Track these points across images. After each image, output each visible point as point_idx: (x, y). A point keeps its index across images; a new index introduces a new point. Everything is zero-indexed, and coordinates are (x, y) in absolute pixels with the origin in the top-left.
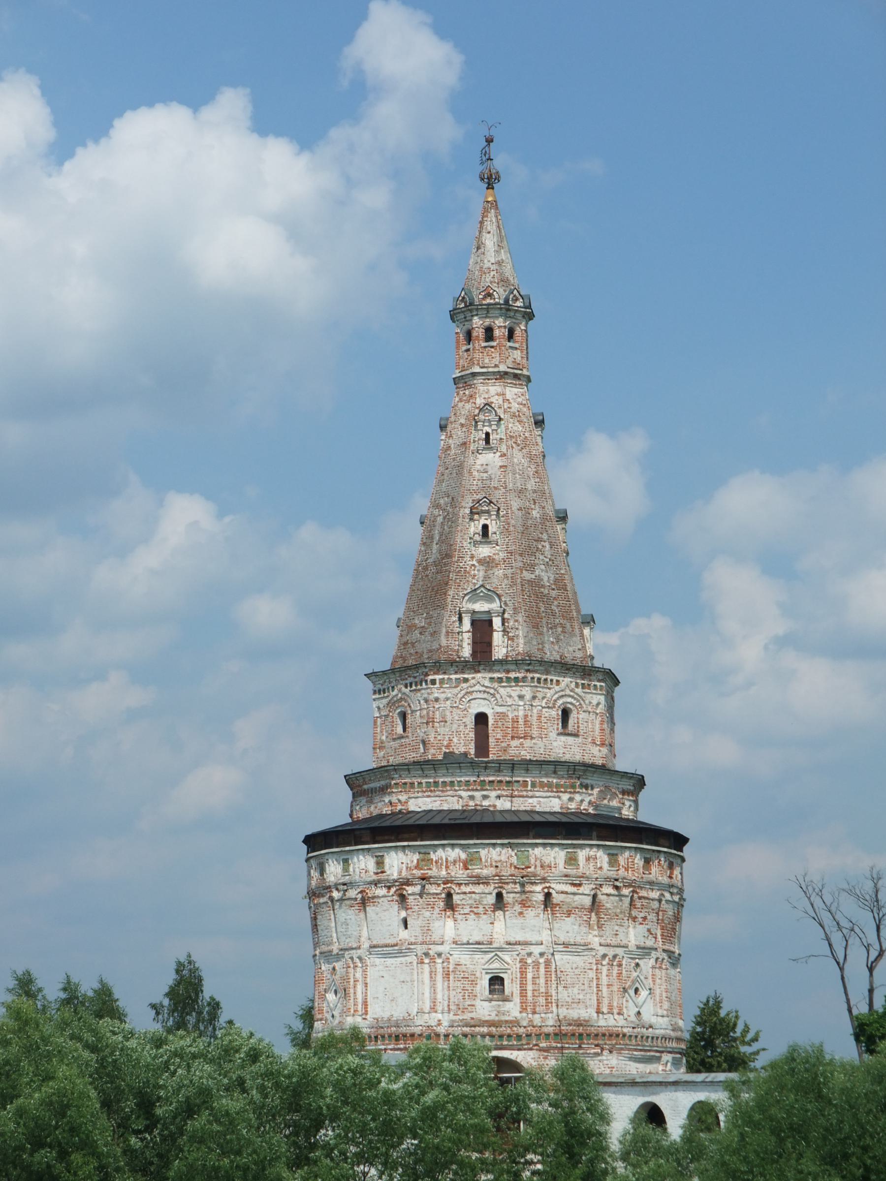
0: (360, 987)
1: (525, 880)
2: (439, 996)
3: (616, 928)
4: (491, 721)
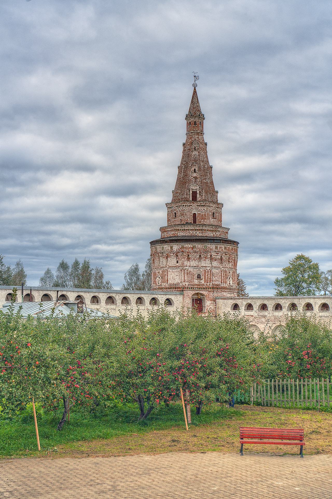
0: (166, 276)
1: (206, 251)
2: (186, 279)
3: (226, 264)
4: (197, 215)
